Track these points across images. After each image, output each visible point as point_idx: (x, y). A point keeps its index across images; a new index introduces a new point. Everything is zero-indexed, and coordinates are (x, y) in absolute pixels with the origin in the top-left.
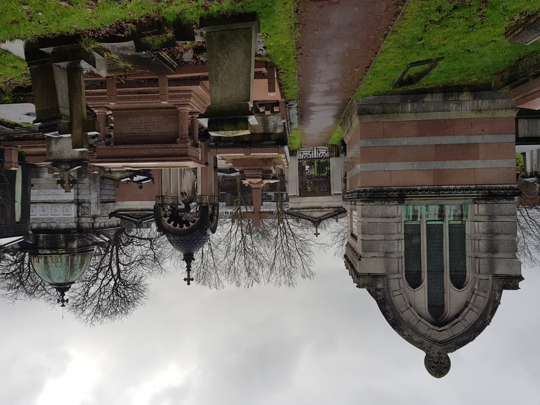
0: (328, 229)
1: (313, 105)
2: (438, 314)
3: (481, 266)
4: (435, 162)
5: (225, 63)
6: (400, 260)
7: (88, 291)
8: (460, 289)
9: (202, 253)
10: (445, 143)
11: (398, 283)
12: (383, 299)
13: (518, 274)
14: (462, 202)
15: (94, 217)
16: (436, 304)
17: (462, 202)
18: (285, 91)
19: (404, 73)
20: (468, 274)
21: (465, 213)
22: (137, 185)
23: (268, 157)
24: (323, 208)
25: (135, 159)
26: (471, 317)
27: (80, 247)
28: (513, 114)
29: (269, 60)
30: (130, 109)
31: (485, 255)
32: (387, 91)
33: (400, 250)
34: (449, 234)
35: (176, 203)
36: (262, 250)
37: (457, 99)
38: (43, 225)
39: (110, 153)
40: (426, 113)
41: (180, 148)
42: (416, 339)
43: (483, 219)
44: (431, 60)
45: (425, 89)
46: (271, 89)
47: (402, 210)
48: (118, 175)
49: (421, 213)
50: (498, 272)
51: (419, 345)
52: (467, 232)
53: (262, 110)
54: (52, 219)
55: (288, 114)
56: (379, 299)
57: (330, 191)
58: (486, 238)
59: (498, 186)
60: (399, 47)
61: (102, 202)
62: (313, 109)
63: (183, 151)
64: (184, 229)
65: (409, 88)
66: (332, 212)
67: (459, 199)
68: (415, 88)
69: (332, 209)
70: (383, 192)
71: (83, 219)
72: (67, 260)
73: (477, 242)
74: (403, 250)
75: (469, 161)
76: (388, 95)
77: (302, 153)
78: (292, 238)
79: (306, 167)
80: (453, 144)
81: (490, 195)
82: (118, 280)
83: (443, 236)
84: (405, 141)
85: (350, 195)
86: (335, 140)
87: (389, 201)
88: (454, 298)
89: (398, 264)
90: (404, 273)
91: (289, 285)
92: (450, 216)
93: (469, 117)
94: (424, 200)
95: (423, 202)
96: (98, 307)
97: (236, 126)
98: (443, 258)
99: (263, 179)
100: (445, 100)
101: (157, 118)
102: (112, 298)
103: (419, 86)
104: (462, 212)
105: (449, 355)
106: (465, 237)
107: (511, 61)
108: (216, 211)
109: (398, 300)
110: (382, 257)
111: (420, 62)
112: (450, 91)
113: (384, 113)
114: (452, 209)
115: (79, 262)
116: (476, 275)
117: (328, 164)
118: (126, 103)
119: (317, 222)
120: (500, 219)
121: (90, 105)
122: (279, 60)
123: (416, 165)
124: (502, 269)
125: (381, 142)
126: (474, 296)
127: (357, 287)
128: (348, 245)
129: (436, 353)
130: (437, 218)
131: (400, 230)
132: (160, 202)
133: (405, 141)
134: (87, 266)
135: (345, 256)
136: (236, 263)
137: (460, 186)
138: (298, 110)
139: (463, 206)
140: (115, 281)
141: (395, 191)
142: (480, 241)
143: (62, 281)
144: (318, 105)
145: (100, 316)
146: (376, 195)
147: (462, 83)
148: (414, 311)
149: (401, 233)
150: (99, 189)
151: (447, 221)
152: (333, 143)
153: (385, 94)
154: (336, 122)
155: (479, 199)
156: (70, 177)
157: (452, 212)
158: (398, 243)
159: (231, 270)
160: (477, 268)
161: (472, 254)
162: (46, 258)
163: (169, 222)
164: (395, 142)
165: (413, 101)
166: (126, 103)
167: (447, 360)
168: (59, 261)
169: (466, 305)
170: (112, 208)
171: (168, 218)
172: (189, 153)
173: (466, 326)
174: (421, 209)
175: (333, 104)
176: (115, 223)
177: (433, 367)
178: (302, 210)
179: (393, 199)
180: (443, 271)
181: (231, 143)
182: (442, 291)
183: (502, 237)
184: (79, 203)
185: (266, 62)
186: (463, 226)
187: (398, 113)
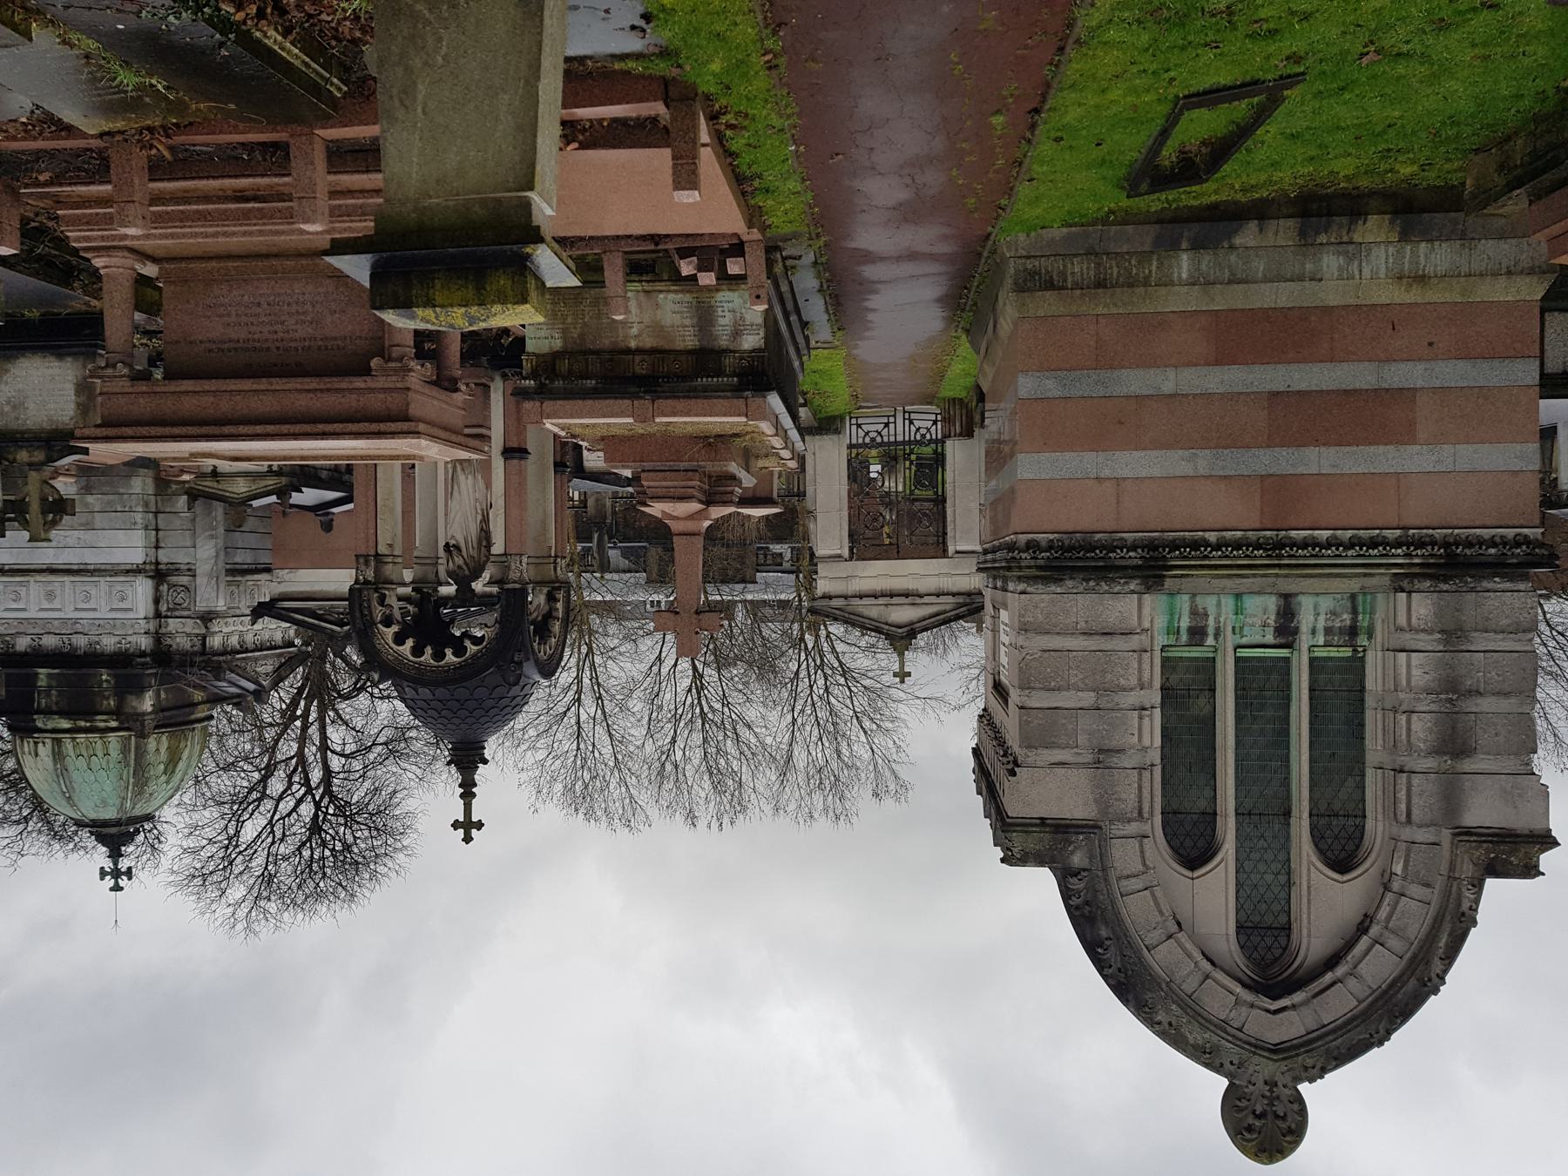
0: (954, 657)
1: (869, 257)
2: (1271, 964)
3: (1415, 800)
4: (1268, 451)
5: (440, 39)
6: (1146, 774)
7: (237, 833)
8: (1342, 872)
9: (578, 723)
10: (1303, 386)
11: (1138, 856)
12: (1087, 903)
13: (1537, 826)
14: (1354, 585)
15: (207, 618)
16: (1267, 931)
17: (1354, 585)
18: (759, 200)
19: (1164, 134)
20: (1369, 824)
21: (1363, 621)
22: (313, 521)
23: (718, 430)
24: (921, 596)
25: (227, 430)
26: (1378, 965)
27: (163, 710)
28: (1535, 290)
29: (675, 72)
30: (219, 257)
31: (1430, 763)
32: (1111, 212)
33: (1146, 742)
34: (1312, 690)
35: (432, 577)
36: (752, 714)
37: (1345, 239)
38: (49, 642)
39: (145, 407)
40: (1241, 286)
41: (384, 390)
42: (1195, 1035)
43: (1424, 641)
44: (1255, 82)
45: (1236, 203)
46: (686, 176)
47: (1153, 609)
48: (241, 487)
49: (1217, 621)
50: (1471, 819)
51: (1206, 1056)
52: (1370, 684)
53: (686, 268)
54: (76, 621)
55: (784, 288)
56: (1075, 901)
57: (944, 543)
58: (1434, 707)
59: (1478, 531)
60: (1139, 22)
61: (232, 572)
62: (870, 272)
63: (393, 402)
64: (448, 665)
65: (1181, 194)
66: (948, 607)
67: (1311, 576)
68: (1206, 200)
69: (950, 599)
70: (1093, 549)
71: (173, 625)
72: (125, 751)
73: (1404, 717)
74: (1158, 742)
75: (1382, 448)
76: (1113, 224)
77: (859, 426)
78: (842, 681)
79: (872, 468)
80: (1328, 392)
81: (1452, 562)
82: (326, 800)
83: (1288, 699)
84: (1168, 381)
85: (989, 557)
86: (956, 383)
87: (1113, 579)
88: (1324, 902)
89: (1141, 787)
90: (1158, 819)
91: (837, 818)
92: (1314, 632)
93: (1384, 300)
94: (1229, 576)
95: (1228, 583)
96: (267, 879)
97: (480, 288)
98: (1288, 767)
99: (709, 502)
100: (1306, 240)
101: (310, 288)
102: (306, 853)
103: (1216, 192)
104: (1355, 620)
105: (1304, 1088)
106: (1363, 700)
107: (1542, 96)
108: (560, 605)
109: (1137, 910)
110: (1085, 766)
111: (1218, 90)
112: (1321, 210)
113: (1100, 284)
114: (1322, 610)
115: (163, 755)
116: (1395, 830)
117: (939, 459)
118: (196, 235)
119: (902, 638)
120: (1481, 642)
121: (78, 240)
122: (708, 72)
123: (1203, 462)
124: (1483, 811)
125: (1088, 385)
126: (1389, 897)
127: (1003, 861)
128: (985, 717)
129: (1260, 1084)
130: (1270, 638)
131: (1146, 675)
132: (370, 574)
133: (1168, 381)
134: (189, 766)
135: (976, 752)
136: (679, 754)
137: (1350, 533)
138: (818, 276)
139: (1360, 598)
140: (317, 805)
141: (1134, 548)
142: (1414, 717)
143: (110, 814)
144: (882, 259)
145: (272, 907)
146: (1074, 560)
147: (1364, 183)
148: (1189, 946)
149: (1151, 686)
150: (221, 530)
151: (1305, 647)
152: (951, 394)
153: (1105, 221)
154: (951, 321)
155: (1415, 575)
156: (47, 490)
157: (1322, 618)
158: (1141, 718)
159: (665, 770)
160: (1403, 807)
161: (1386, 760)
162: (58, 742)
163: (399, 639)
164: (1134, 381)
165: (1197, 246)
166: (196, 235)
167: (1296, 1107)
168: (100, 754)
169: (1362, 928)
170: (266, 588)
171: (395, 628)
172: (414, 410)
173: (1361, 997)
174: (1219, 608)
175: (932, 257)
176: (278, 637)
177: (1250, 1129)
178: (857, 601)
179: (1126, 572)
180: (1288, 814)
181: (590, 383)
182: (1283, 879)
183: (1486, 704)
184: (159, 574)
185: (666, 83)
186: (1356, 666)
187: (1146, 283)
